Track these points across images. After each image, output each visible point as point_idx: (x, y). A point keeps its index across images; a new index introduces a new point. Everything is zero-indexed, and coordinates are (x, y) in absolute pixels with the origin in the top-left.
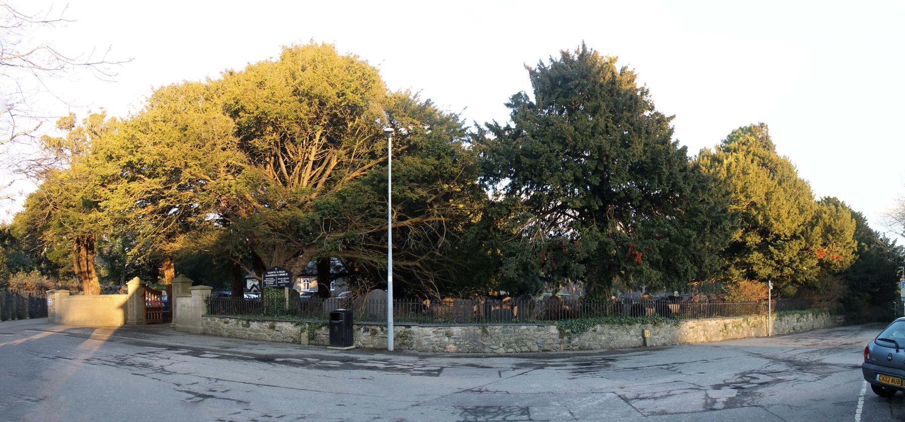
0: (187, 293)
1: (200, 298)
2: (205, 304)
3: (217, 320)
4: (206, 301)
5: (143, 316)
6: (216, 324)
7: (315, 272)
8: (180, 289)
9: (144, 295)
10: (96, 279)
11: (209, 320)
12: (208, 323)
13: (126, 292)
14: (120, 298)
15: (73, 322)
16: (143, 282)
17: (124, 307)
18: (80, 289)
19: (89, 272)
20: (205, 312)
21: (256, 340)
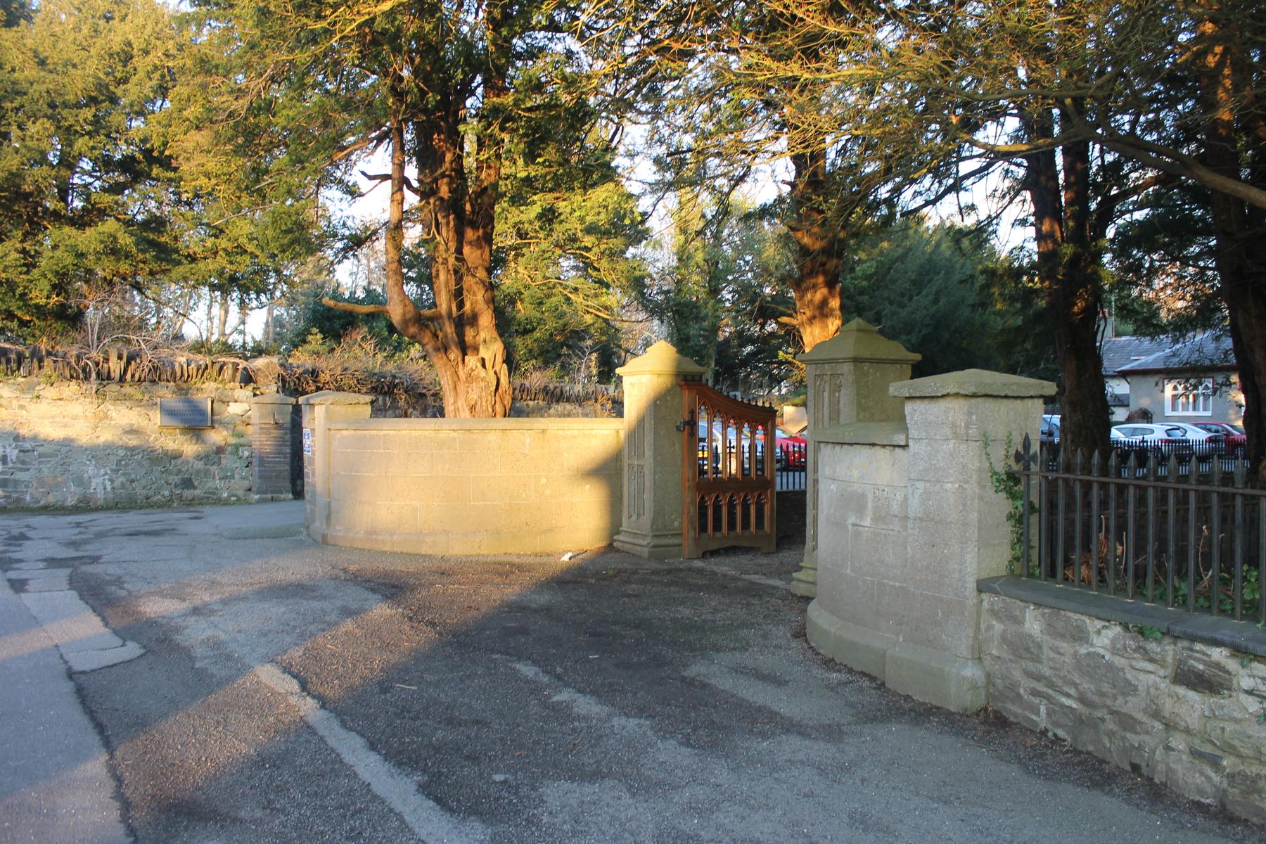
0: (881, 421)
1: (970, 459)
2: (1002, 505)
3: (1104, 637)
4: (1011, 481)
5: (681, 517)
6: (1092, 666)
7: (1233, 360)
8: (846, 398)
9: (692, 424)
10: (492, 350)
11: (1033, 623)
12: (1023, 648)
13: (617, 407)
14: (596, 435)
15: (372, 532)
16: (692, 366)
17: (608, 471)
18: (435, 395)
19: (464, 322)
20: (999, 558)
21: (1204, 662)
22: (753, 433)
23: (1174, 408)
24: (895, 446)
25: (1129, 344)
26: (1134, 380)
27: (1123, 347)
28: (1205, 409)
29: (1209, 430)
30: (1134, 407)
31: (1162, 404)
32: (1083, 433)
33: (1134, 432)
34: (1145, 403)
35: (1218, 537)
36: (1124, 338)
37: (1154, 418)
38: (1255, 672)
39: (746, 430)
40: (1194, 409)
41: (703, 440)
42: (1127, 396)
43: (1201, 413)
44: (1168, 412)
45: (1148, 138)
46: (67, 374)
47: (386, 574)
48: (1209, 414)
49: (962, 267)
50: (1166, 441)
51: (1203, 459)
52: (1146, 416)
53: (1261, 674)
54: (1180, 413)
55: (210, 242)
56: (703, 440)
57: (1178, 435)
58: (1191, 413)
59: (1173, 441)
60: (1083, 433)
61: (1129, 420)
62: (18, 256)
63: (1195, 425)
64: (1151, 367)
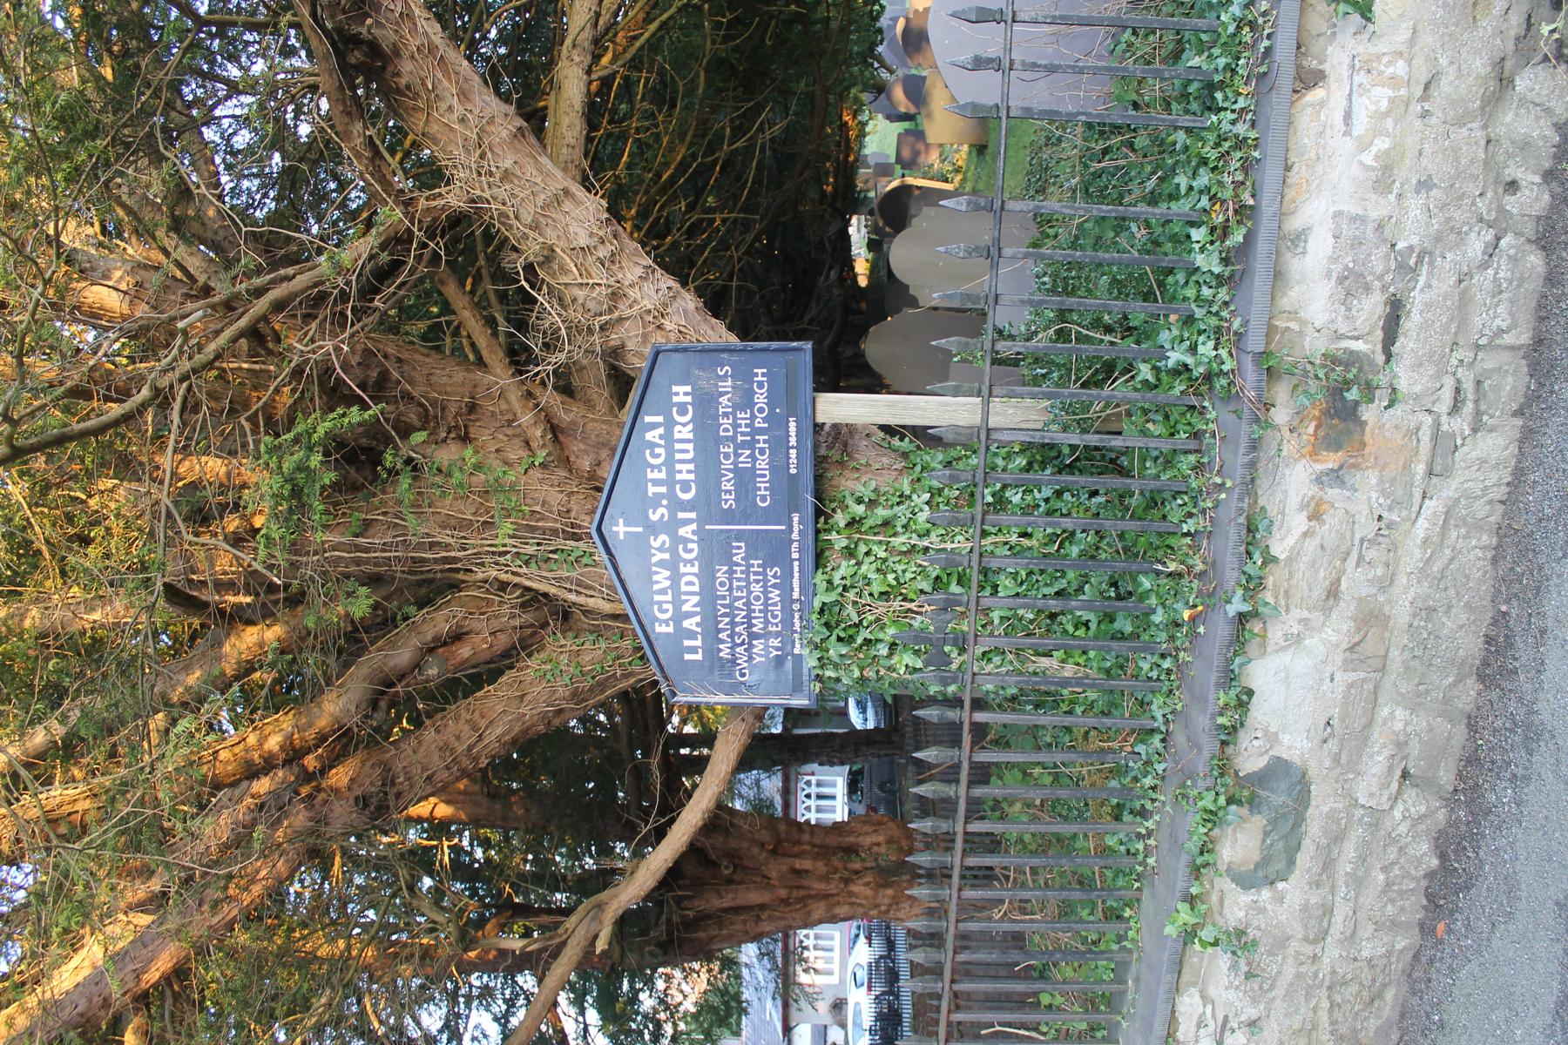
22: (677, 394)
23: (830, 973)
28: (832, 938)
29: (857, 936)
35: (1010, 830)
37: (841, 996)
38: (1191, 1035)
39: (691, 467)
41: (774, 586)
42: (814, 1027)
43: (836, 943)
47: (663, 871)
49: (351, 164)
50: (870, 988)
51: (891, 945)
52: (838, 1006)
53: (1193, 1029)
54: (836, 966)
55: (1392, 197)
56: (774, 586)
57: (862, 975)
58: (836, 954)
59: (870, 979)
61: (843, 1026)
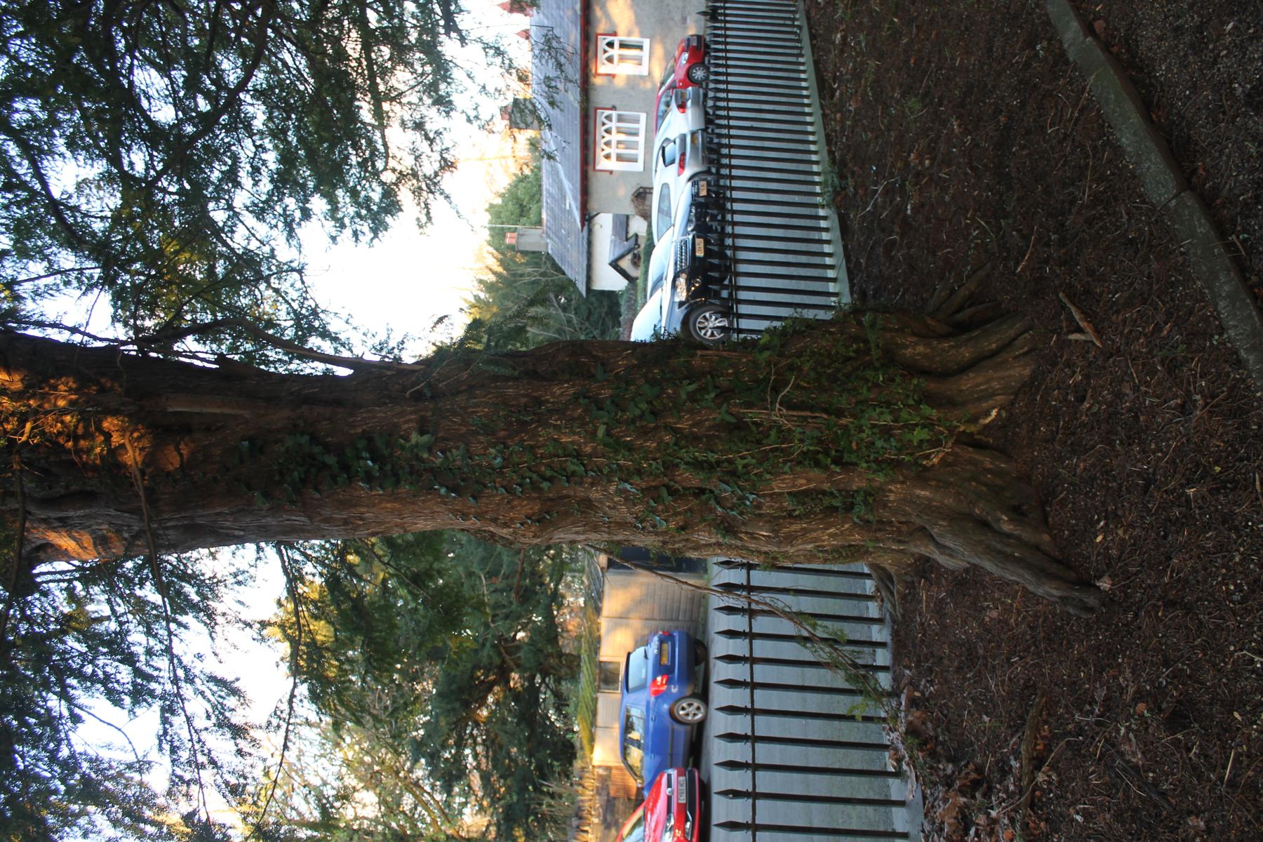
24: (588, 37)
25: (552, 210)
26: (594, 205)
27: (554, 218)
28: (637, 121)
30: (629, 209)
31: (624, 174)
32: (688, 477)
33: (665, 212)
34: (625, 193)
36: (544, 216)
37: (645, 185)
40: (637, 121)
42: (616, 217)
43: (642, 126)
44: (638, 167)
45: (269, 30)
46: (89, 684)
48: (643, 117)
50: (682, 166)
54: (640, 153)
58: (641, 139)
59: (683, 155)
60: (688, 477)
61: (646, 216)
62: (634, 791)
63: (657, 129)
64: (578, 185)
